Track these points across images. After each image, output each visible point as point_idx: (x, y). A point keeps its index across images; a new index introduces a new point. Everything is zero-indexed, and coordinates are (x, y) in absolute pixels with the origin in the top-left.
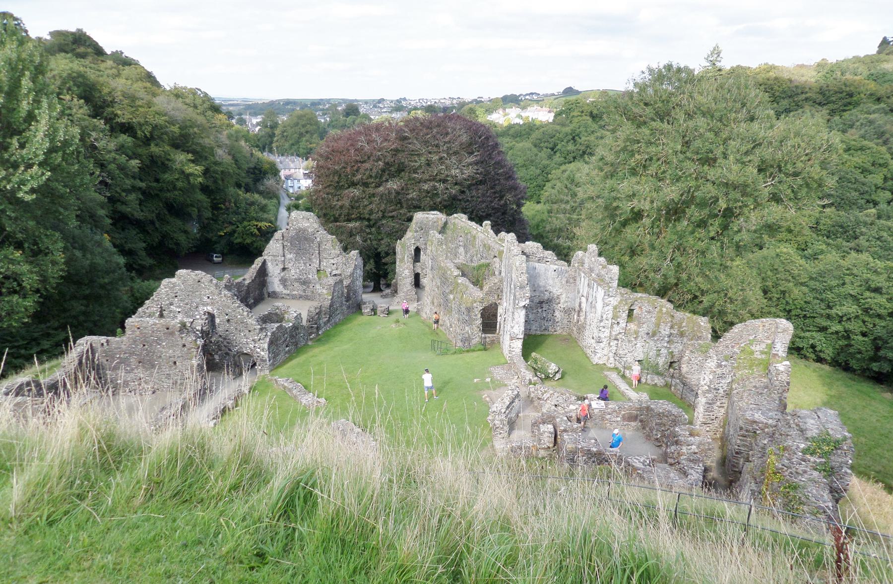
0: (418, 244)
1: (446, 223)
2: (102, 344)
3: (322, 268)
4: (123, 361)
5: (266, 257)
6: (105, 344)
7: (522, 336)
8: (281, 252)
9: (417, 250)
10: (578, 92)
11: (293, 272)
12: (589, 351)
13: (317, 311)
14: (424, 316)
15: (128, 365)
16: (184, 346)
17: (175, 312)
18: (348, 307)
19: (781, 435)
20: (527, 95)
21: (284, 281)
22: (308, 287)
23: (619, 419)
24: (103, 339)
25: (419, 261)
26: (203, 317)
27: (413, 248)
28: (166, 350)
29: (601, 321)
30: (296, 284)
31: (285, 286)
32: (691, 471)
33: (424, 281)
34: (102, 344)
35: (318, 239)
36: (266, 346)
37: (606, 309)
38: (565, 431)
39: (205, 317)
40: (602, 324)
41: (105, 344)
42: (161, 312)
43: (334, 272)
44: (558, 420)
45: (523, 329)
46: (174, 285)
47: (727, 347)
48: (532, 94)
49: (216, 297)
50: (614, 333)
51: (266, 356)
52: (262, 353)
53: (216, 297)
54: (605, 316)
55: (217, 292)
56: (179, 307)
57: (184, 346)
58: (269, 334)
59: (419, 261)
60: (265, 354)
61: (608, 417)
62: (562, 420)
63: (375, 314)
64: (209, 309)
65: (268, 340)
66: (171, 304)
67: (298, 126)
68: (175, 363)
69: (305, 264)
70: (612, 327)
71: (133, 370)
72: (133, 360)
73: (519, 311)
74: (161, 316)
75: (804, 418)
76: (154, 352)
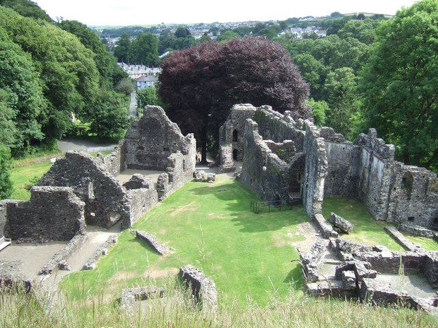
10: (341, 15)
20: (305, 18)
21: (139, 157)
29: (381, 187)
31: (140, 161)
48: (309, 17)
54: (384, 183)
72: (35, 217)
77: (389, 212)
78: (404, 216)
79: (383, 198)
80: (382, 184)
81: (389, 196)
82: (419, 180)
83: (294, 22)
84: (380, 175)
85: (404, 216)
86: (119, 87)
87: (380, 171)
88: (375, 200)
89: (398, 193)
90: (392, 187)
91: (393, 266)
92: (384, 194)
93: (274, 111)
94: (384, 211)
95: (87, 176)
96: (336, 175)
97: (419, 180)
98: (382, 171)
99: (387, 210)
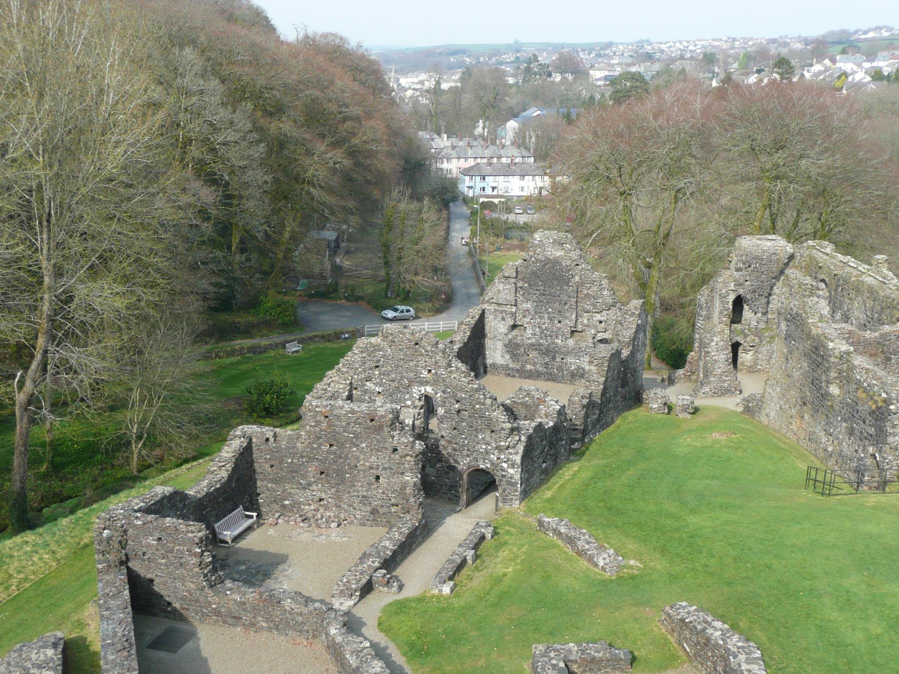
0: (741, 291)
1: (792, 257)
2: (267, 439)
3: (579, 328)
4: (294, 471)
5: (486, 306)
6: (271, 440)
8: (511, 298)
9: (739, 303)
11: (529, 331)
13: (585, 401)
15: (304, 477)
16: (395, 450)
17: (372, 392)
18: (624, 398)
19: (390, 468)
21: (512, 348)
22: (554, 358)
24: (268, 431)
25: (739, 322)
26: (418, 403)
27: (732, 297)
28: (368, 458)
30: (533, 354)
31: (514, 356)
33: (727, 354)
34: (267, 439)
35: (577, 278)
36: (518, 459)
39: (418, 403)
41: (271, 440)
42: (350, 391)
43: (600, 336)
46: (377, 348)
48: (879, 28)
49: (442, 371)
51: (517, 477)
52: (511, 471)
53: (442, 371)
55: (443, 363)
56: (380, 384)
57: (395, 450)
58: (523, 438)
59: (739, 322)
60: (515, 473)
64: (429, 389)
65: (521, 448)
66: (369, 379)
67: (483, 95)
68: (378, 478)
69: (550, 319)
71: (309, 484)
72: (312, 470)
74: (350, 398)
76: (346, 458)
83: (847, 44)
95: (427, 383)
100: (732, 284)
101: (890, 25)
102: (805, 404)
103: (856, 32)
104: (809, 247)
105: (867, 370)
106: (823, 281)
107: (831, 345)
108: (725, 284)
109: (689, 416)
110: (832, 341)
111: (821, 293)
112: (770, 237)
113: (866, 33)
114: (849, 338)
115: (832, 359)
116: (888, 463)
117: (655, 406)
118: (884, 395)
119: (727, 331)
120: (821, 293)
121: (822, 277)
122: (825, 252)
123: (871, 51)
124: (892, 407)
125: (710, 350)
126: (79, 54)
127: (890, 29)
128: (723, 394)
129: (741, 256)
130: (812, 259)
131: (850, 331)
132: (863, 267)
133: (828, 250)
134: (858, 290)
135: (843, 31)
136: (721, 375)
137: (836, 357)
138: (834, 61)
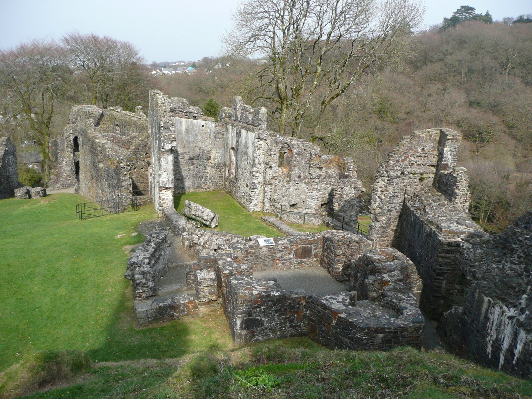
1: (102, 115)
7: (171, 186)
12: (244, 201)
14: (81, 193)
23: (291, 256)
27: (72, 138)
29: (254, 166)
32: (403, 304)
37: (258, 152)
38: (231, 274)
40: (255, 169)
44: (220, 262)
45: (172, 177)
47: (398, 161)
48: (180, 61)
50: (267, 178)
54: (257, 161)
61: (279, 255)
62: (225, 261)
63: (30, 197)
70: (265, 173)
73: (166, 155)
75: (257, 360)
77: (266, 200)
78: (285, 203)
79: (256, 181)
80: (254, 161)
81: (264, 178)
82: (299, 154)
83: (166, 66)
84: (250, 150)
85: (285, 203)
86: (226, 358)
87: (250, 145)
88: (247, 186)
89: (276, 172)
90: (268, 165)
91: (278, 259)
92: (257, 175)
93: (124, 112)
94: (260, 198)
96: (195, 162)
97: (299, 154)
98: (253, 143)
99: (264, 196)
100: (71, 130)
101: (184, 60)
102: (93, 178)
103: (171, 63)
104: (111, 110)
105: (112, 148)
106: (117, 125)
107: (97, 141)
108: (68, 130)
109: (39, 198)
110: (98, 139)
111: (118, 132)
112: (90, 106)
113: (175, 63)
114: (113, 140)
115: (99, 149)
116: (124, 198)
117: (18, 195)
118: (118, 159)
119: (72, 156)
120: (118, 132)
121: (116, 123)
122: (118, 111)
123: (175, 67)
124: (122, 165)
125: (62, 166)
126: (345, 333)
127: (183, 62)
128: (68, 187)
129: (74, 115)
130: (112, 115)
131: (113, 136)
132: (132, 114)
133: (119, 110)
134: (130, 125)
135: (166, 62)
136: (67, 177)
137: (100, 147)
138: (161, 70)
